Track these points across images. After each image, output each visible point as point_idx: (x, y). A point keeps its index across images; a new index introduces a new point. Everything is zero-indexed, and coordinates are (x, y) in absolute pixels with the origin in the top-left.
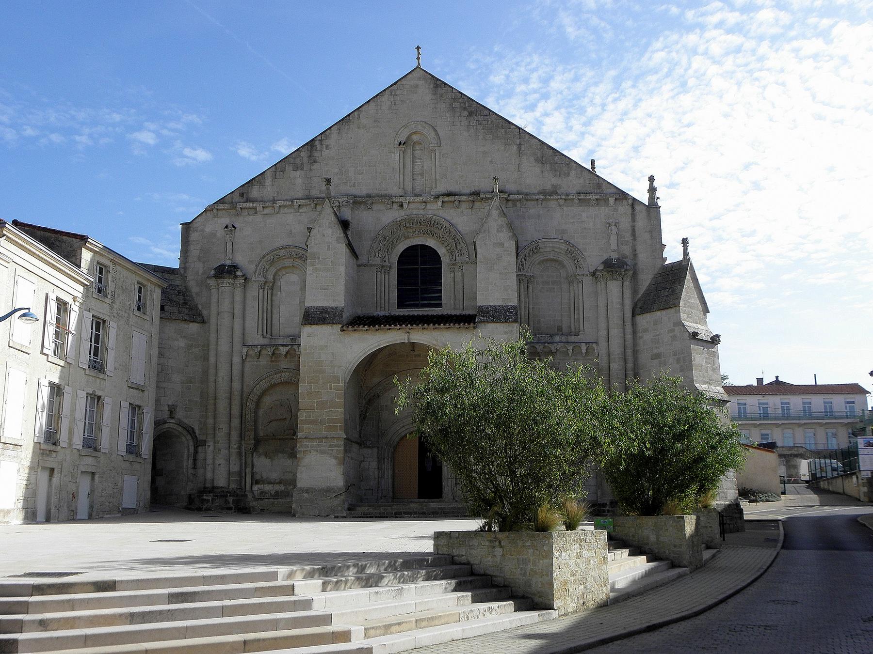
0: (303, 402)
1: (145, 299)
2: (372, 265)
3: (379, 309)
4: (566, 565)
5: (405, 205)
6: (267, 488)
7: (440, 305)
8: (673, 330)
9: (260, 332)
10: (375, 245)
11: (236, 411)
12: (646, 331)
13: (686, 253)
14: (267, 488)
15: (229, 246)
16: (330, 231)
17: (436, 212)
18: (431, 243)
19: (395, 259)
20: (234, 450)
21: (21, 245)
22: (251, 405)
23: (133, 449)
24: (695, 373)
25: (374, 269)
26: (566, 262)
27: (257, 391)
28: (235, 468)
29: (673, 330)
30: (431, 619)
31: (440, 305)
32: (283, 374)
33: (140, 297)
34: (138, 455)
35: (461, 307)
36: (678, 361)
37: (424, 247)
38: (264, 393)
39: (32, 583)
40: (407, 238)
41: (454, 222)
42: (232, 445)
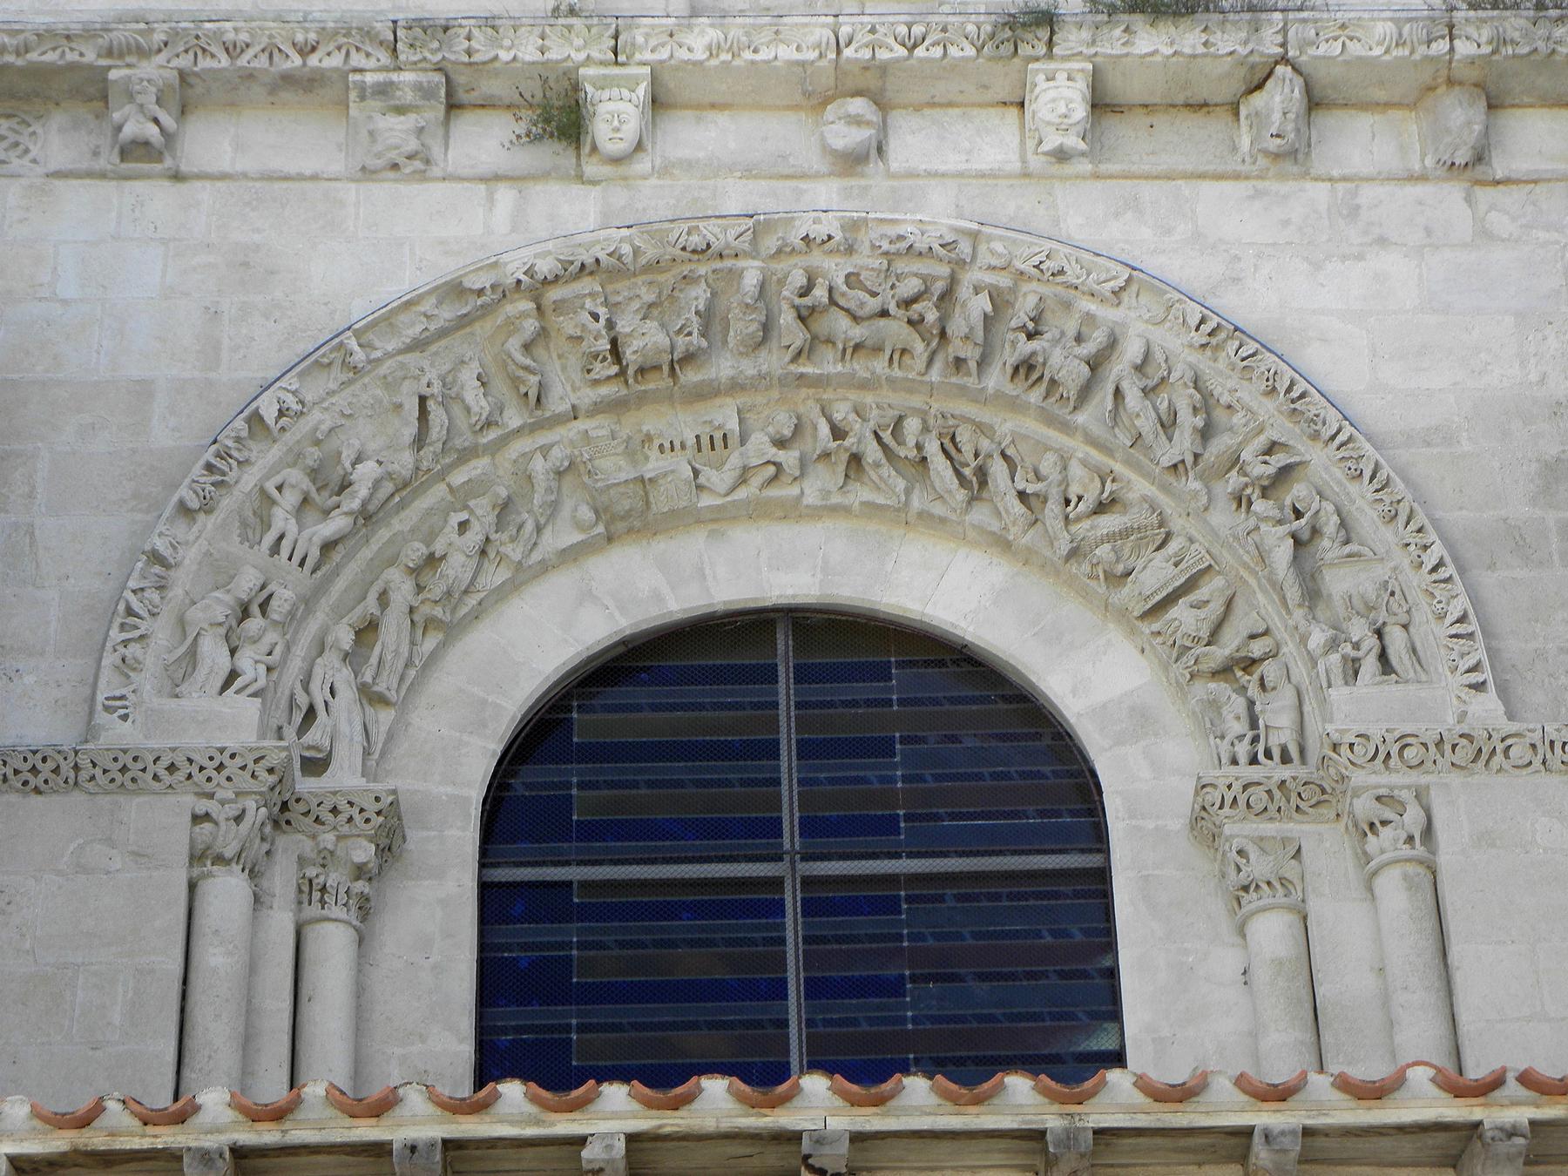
2: (128, 773)
5: (616, 115)
10: (193, 546)
17: (1011, 204)
18: (946, 585)
19: (448, 758)
25: (163, 819)
30: (983, 176)
40: (627, 519)
41: (1250, 305)
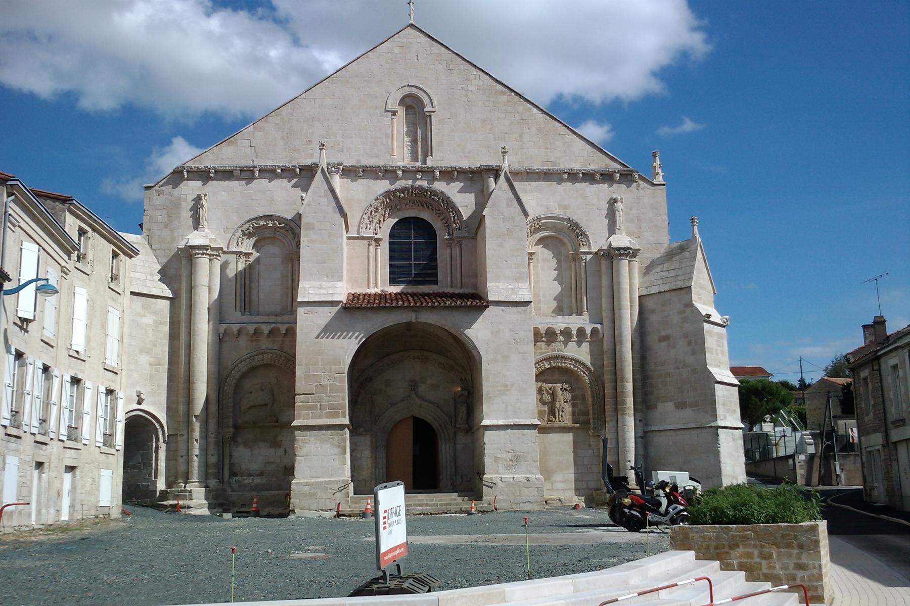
0: (299, 387)
3: (371, 285)
4: (475, 78)
6: (248, 481)
8: (684, 312)
9: (238, 308)
12: (653, 312)
13: (498, 303)
14: (248, 481)
16: (325, 200)
18: (425, 215)
20: (212, 440)
21: (26, 206)
23: (108, 438)
26: (566, 241)
27: (236, 374)
28: (213, 460)
32: (266, 355)
34: (112, 445)
35: (459, 285)
36: (689, 344)
38: (244, 376)
39: (430, 542)
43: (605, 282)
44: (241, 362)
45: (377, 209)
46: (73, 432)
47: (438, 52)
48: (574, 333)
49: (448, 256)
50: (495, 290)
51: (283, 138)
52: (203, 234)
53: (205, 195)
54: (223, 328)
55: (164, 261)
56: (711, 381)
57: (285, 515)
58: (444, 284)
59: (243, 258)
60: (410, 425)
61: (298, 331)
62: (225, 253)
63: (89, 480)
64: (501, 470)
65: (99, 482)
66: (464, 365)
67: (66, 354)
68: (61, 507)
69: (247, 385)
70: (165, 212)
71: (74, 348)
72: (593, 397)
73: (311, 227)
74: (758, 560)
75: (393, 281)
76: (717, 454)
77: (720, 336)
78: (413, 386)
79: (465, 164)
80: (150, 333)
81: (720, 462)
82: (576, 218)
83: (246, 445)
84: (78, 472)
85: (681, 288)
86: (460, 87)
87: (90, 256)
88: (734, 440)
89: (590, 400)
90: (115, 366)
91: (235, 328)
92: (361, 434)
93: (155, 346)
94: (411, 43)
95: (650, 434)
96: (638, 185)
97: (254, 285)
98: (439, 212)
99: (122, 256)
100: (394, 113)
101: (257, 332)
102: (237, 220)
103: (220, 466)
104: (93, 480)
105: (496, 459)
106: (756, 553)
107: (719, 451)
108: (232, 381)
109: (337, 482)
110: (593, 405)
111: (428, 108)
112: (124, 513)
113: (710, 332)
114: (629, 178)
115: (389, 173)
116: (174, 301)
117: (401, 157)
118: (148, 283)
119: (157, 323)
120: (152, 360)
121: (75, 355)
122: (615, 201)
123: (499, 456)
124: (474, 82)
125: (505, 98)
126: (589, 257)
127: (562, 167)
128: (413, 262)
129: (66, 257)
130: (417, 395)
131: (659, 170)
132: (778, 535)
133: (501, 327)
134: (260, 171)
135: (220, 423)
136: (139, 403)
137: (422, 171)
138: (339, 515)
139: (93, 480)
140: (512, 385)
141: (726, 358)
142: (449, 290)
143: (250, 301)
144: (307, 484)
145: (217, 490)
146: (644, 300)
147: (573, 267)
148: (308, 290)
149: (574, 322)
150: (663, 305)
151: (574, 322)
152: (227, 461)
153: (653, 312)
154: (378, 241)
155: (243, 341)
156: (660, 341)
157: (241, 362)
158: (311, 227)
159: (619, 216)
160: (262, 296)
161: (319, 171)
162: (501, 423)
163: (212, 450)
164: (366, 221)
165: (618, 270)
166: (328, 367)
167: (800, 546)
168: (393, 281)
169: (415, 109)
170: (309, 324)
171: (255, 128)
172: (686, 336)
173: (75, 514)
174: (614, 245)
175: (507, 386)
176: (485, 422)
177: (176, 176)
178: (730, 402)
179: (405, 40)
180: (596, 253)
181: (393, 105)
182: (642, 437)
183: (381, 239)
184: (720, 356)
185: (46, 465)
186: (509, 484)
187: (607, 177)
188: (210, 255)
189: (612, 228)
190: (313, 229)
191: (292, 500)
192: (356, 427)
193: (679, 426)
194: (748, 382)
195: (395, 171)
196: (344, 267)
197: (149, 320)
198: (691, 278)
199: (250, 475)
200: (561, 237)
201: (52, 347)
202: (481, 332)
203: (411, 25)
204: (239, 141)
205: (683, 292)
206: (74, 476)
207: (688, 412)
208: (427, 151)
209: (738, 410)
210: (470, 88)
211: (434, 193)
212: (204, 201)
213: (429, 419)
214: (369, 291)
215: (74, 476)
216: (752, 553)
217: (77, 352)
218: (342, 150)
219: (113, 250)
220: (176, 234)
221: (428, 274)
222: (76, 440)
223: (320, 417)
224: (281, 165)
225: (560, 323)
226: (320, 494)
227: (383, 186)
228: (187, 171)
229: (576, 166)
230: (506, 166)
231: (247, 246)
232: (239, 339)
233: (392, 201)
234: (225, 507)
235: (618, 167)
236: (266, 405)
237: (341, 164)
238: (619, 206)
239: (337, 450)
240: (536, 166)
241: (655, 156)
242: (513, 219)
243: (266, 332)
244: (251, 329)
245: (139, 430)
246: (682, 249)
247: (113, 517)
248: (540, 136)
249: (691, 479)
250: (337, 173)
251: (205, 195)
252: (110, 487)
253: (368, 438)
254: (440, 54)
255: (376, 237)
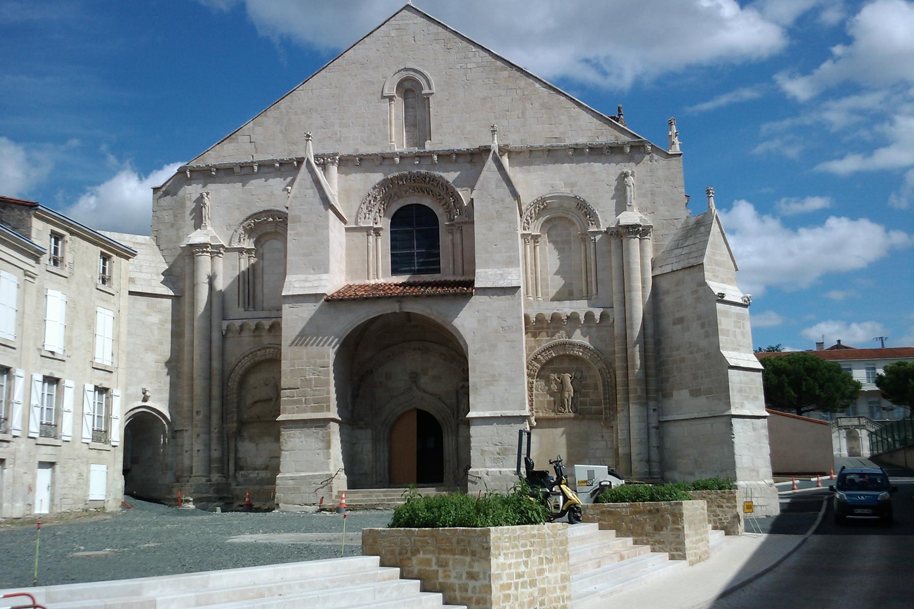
0: (284, 383)
1: (110, 271)
3: (371, 276)
4: (475, 56)
6: (253, 475)
7: (438, 271)
8: (696, 292)
11: (216, 392)
12: (667, 292)
13: (485, 291)
14: (253, 475)
15: (652, 387)
18: (427, 202)
20: (215, 434)
22: (233, 384)
23: (101, 435)
24: (722, 338)
27: (239, 371)
28: (216, 454)
29: (696, 292)
31: (438, 271)
33: (104, 269)
35: (460, 271)
37: (419, 206)
38: (248, 371)
42: (212, 429)
43: (614, 263)
44: (244, 358)
45: (376, 198)
46: (50, 430)
47: (435, 31)
48: (582, 318)
49: (450, 243)
50: (484, 277)
51: (282, 132)
52: (205, 232)
53: (208, 194)
54: (225, 324)
55: (171, 260)
56: (719, 368)
57: (269, 510)
58: (447, 273)
59: (245, 255)
60: (414, 417)
61: (283, 325)
62: (227, 250)
63: (75, 476)
64: (488, 463)
65: (88, 477)
66: (454, 354)
67: (37, 354)
68: (33, 501)
69: (253, 380)
70: (171, 212)
71: (47, 348)
72: (604, 385)
73: (297, 220)
74: (435, 568)
75: (395, 271)
76: (731, 445)
77: (740, 316)
78: (414, 378)
79: (464, 146)
80: (156, 332)
81: (734, 454)
82: (583, 196)
83: (251, 439)
84: (57, 467)
85: (693, 266)
86: (458, 66)
87: (68, 258)
88: (754, 429)
89: (601, 389)
90: (110, 364)
91: (237, 323)
92: (361, 428)
93: (161, 344)
94: (407, 24)
95: (666, 424)
96: (652, 157)
97: (258, 281)
98: (439, 198)
99: (115, 258)
100: (391, 98)
101: (258, 327)
102: (238, 217)
103: (223, 462)
104: (81, 475)
105: (483, 452)
106: (434, 560)
107: (733, 443)
108: (236, 377)
109: (321, 476)
110: (605, 394)
111: (426, 91)
112: (124, 505)
113: (726, 314)
114: (642, 149)
115: (384, 159)
116: (177, 299)
117: (398, 142)
118: (154, 283)
119: (162, 322)
120: (158, 357)
121: (50, 355)
122: (626, 175)
123: (486, 449)
124: (474, 60)
125: (506, 74)
126: (598, 237)
127: (568, 142)
128: (416, 251)
129: (32, 262)
130: (419, 388)
131: (676, 140)
132: (454, 540)
133: (488, 314)
134: (259, 166)
135: (223, 419)
136: (145, 400)
137: (419, 156)
138: (321, 510)
139: (81, 475)
140: (500, 375)
141: (749, 340)
142: (451, 278)
143: (254, 297)
144: (292, 479)
145: (218, 484)
146: (658, 279)
147: (583, 247)
148: (294, 284)
149: (580, 307)
150: (677, 285)
151: (580, 307)
152: (232, 455)
153: (667, 292)
154: (377, 232)
155: (246, 337)
156: (674, 324)
157: (244, 358)
158: (297, 220)
159: (631, 192)
160: (265, 291)
161: (305, 163)
162: (487, 414)
163: (215, 445)
164: (365, 210)
165: (628, 249)
166: (312, 361)
167: (473, 554)
168: (395, 271)
169: (411, 91)
170: (294, 318)
171: (254, 124)
172: (699, 318)
173: (55, 508)
174: (622, 222)
175: (494, 376)
176: (471, 414)
177: (181, 176)
178: (751, 388)
179: (401, 22)
180: (606, 232)
181: (391, 89)
182: (657, 428)
183: (380, 229)
184: (740, 338)
185: (7, 462)
186: (495, 478)
187: (613, 151)
188: (211, 253)
189: (622, 205)
190: (300, 221)
191: (277, 495)
192: (351, 421)
193: (696, 415)
194: (905, 364)
195: (393, 158)
196: (341, 256)
197: (154, 319)
198: (703, 255)
199: (256, 469)
200: (563, 219)
201: (14, 348)
202: (468, 321)
203: (408, 7)
204: (240, 138)
205: (696, 269)
206: (54, 472)
207: (702, 401)
208: (427, 135)
209: (762, 397)
210: (469, 66)
211: (433, 179)
212: (206, 200)
213: (432, 411)
214: (367, 282)
215: (54, 472)
216: (431, 560)
217: (52, 353)
218: (340, 140)
219: (102, 253)
220: (181, 234)
221: (431, 263)
222: (55, 437)
223: (305, 411)
224: (278, 158)
225: (566, 308)
226: (303, 488)
227: (378, 177)
228: (190, 171)
229: (582, 140)
230: (495, 146)
231: (249, 244)
232: (242, 335)
233: (389, 190)
234: (227, 501)
235: (627, 139)
236: (271, 399)
237: (337, 154)
238: (630, 180)
239: (321, 445)
240: (539, 142)
241: (671, 124)
242: (503, 200)
243: (267, 327)
244: (252, 324)
245: (140, 427)
246: (698, 224)
247: (108, 510)
248: (544, 111)
249: (610, 473)
250: (333, 164)
251: (208, 194)
252: (105, 480)
253: (369, 431)
254: (438, 33)
255: (376, 226)
